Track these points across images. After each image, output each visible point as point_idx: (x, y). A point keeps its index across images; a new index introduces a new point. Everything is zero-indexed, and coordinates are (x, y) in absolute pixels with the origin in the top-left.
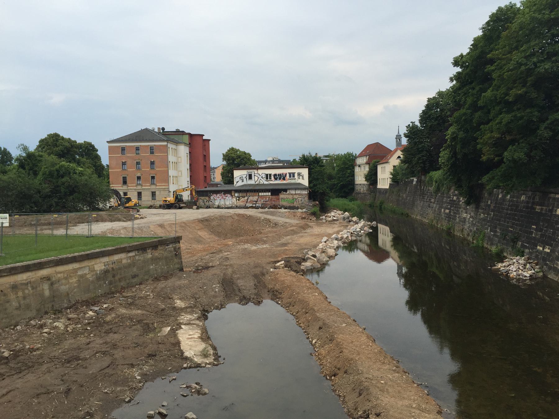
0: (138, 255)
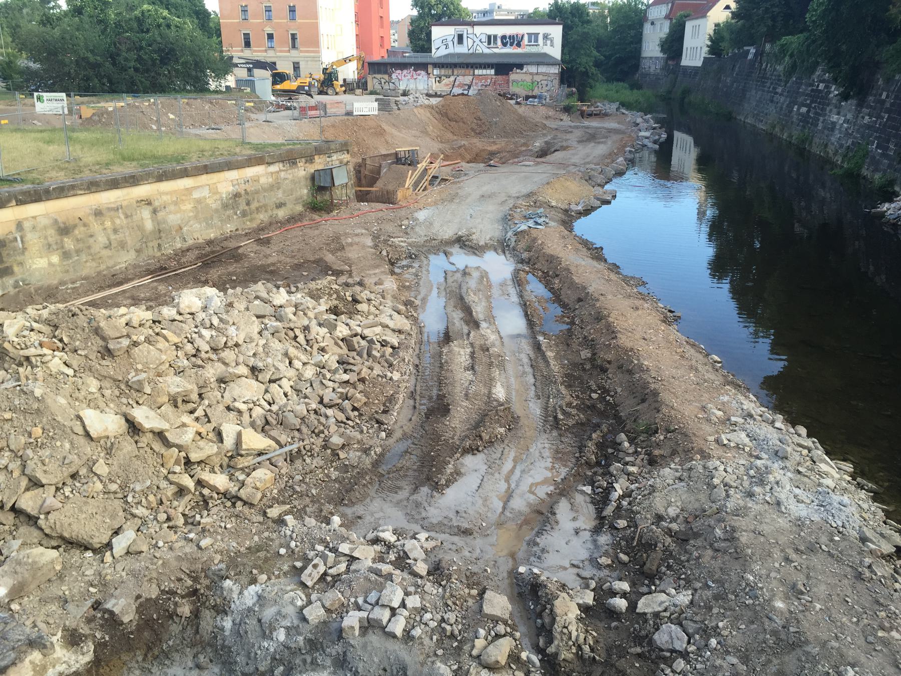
0: (283, 171)
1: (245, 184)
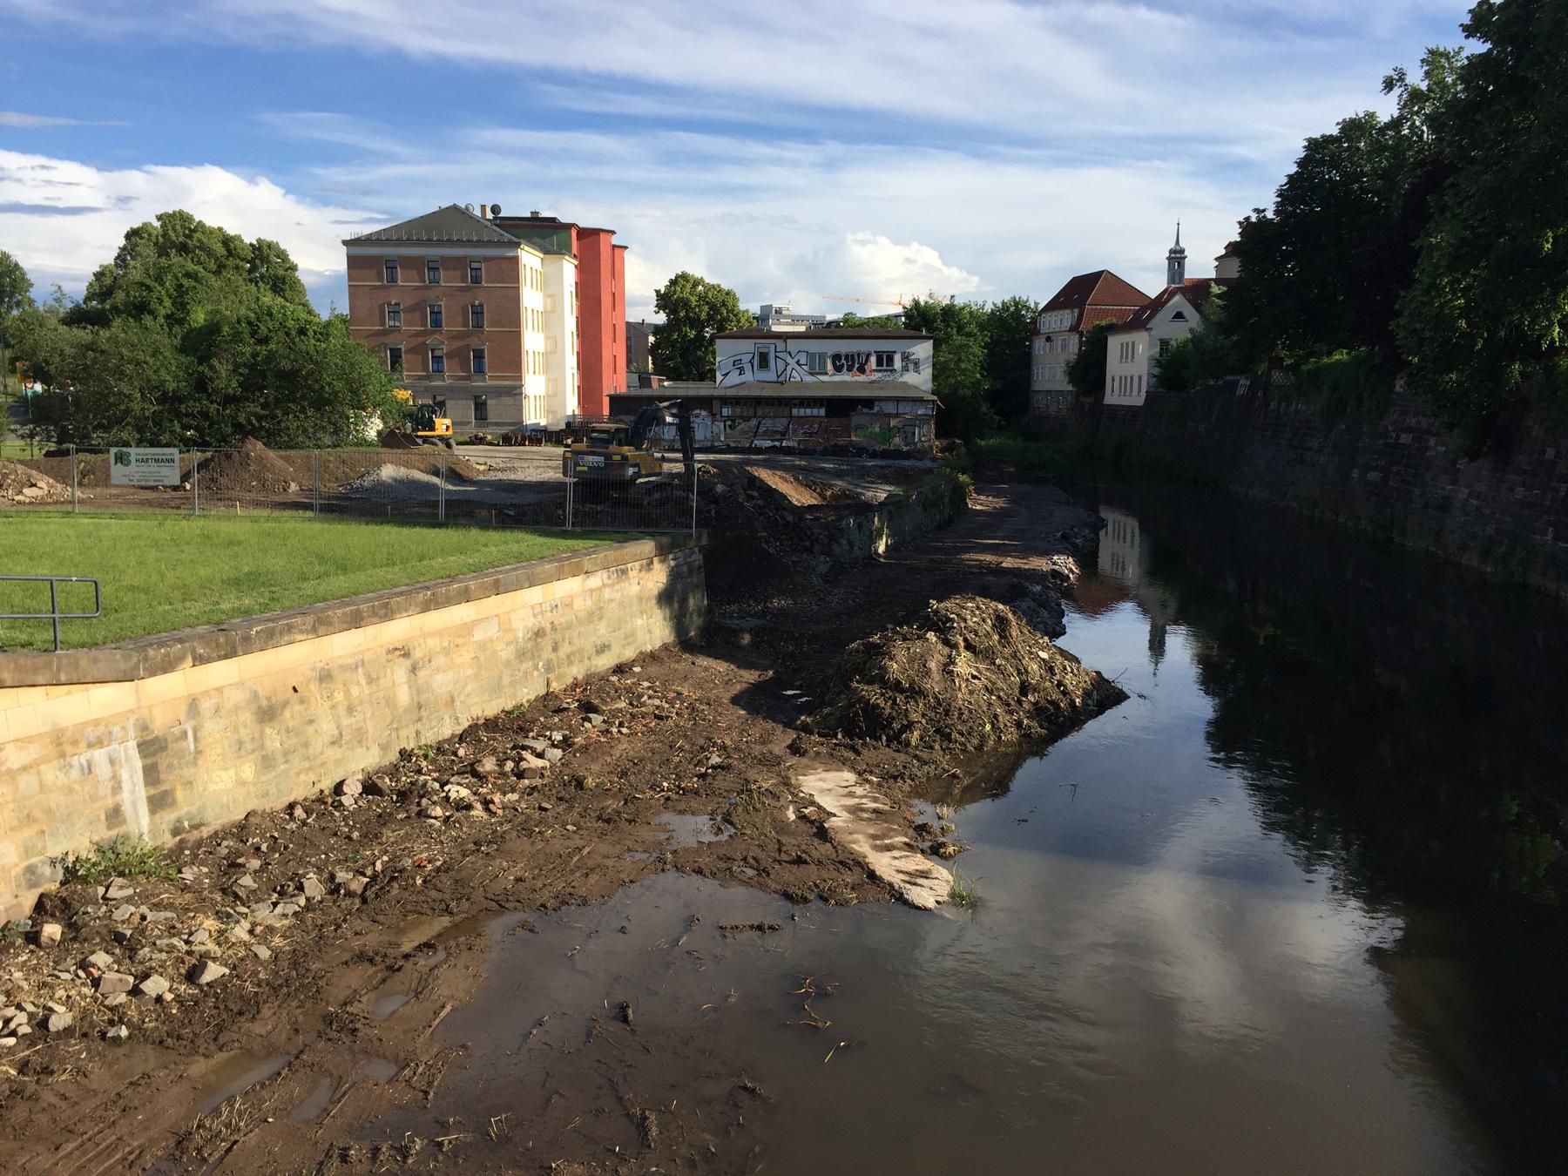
0: (608, 585)
1: (552, 611)
